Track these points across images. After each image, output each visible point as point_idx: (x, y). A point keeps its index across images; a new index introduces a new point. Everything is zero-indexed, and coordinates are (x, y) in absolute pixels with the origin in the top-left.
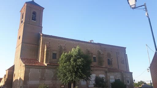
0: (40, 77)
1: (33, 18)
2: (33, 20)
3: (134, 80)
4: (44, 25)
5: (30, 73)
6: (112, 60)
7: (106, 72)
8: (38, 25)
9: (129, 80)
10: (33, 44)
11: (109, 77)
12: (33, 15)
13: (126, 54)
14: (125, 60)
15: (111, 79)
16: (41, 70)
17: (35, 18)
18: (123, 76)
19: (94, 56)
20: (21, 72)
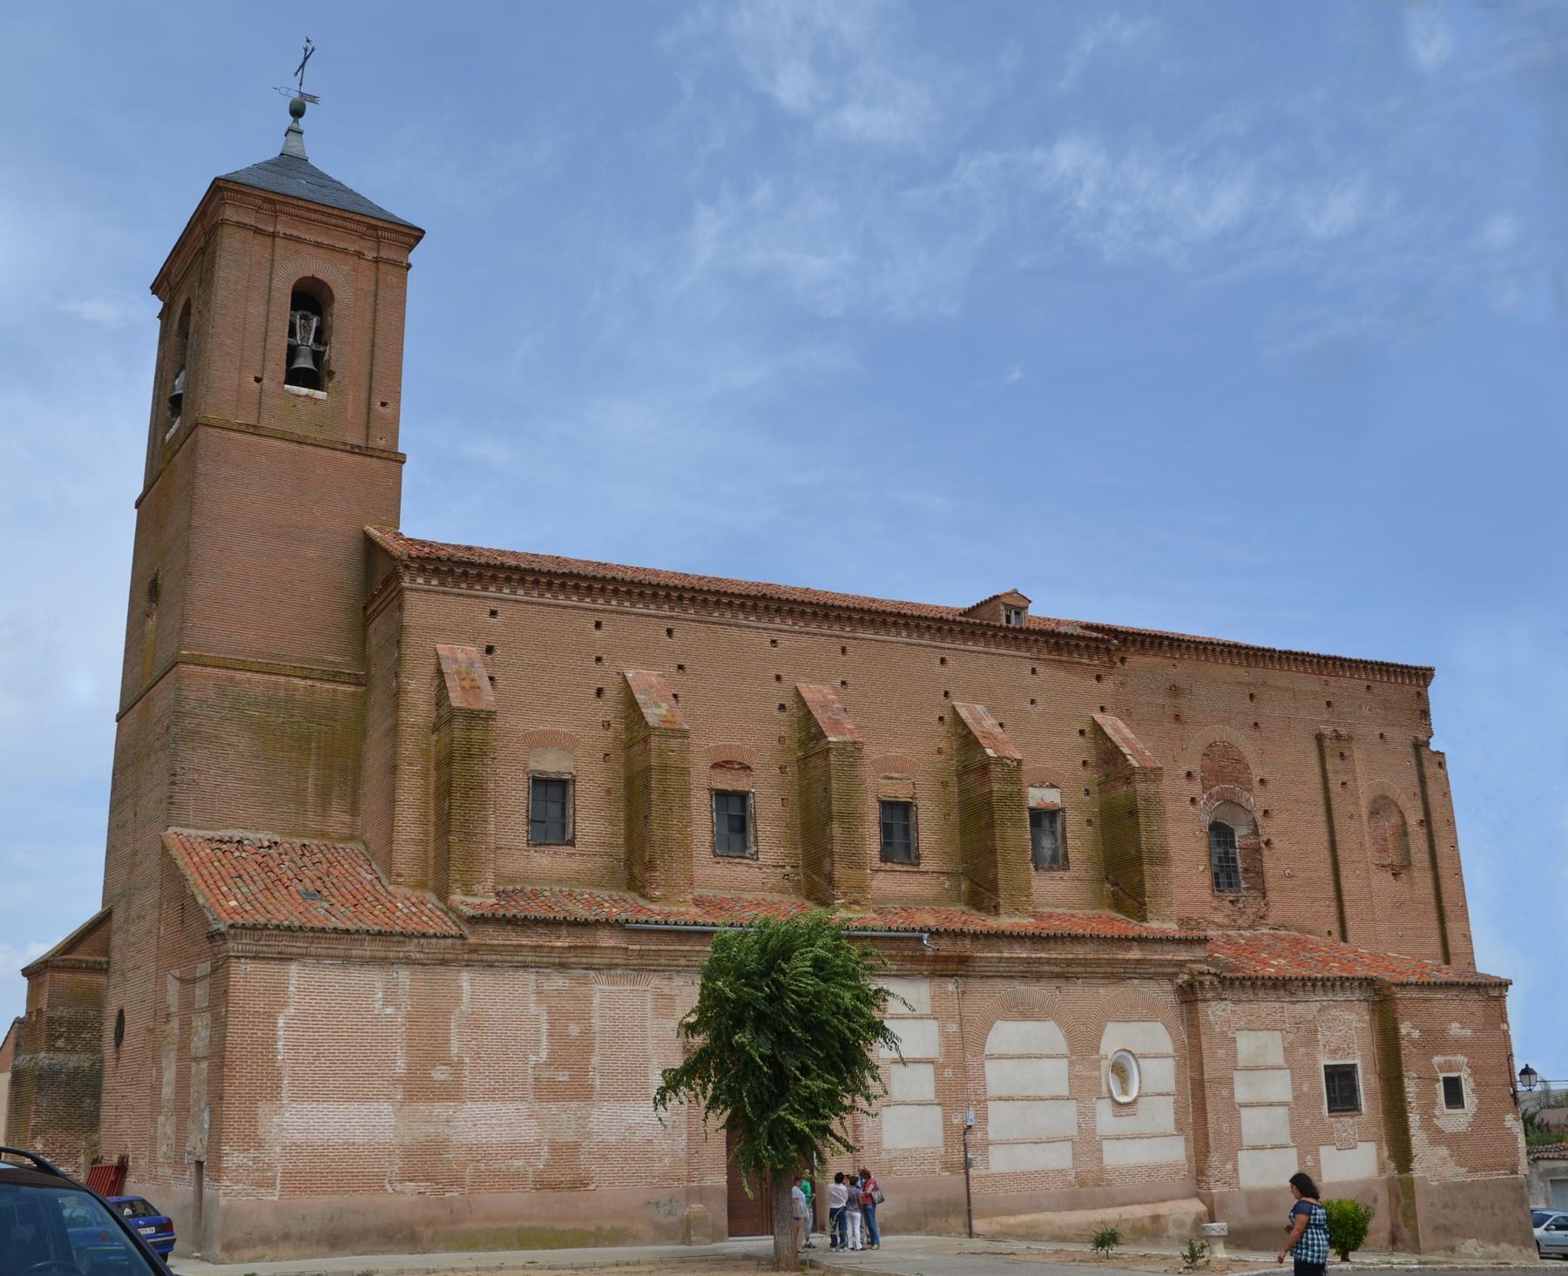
0: (401, 1066)
1: (292, 353)
2: (294, 376)
3: (1527, 1071)
4: (417, 434)
5: (291, 1011)
6: (1268, 830)
7: (1189, 995)
8: (355, 439)
9: (1464, 1075)
10: (334, 677)
11: (1229, 1082)
12: (274, 302)
13: (1435, 745)
14: (1427, 822)
15: (1058, 1056)
16: (404, 976)
17: (317, 357)
18: (1396, 1030)
19: (1041, 796)
20: (187, 1005)
